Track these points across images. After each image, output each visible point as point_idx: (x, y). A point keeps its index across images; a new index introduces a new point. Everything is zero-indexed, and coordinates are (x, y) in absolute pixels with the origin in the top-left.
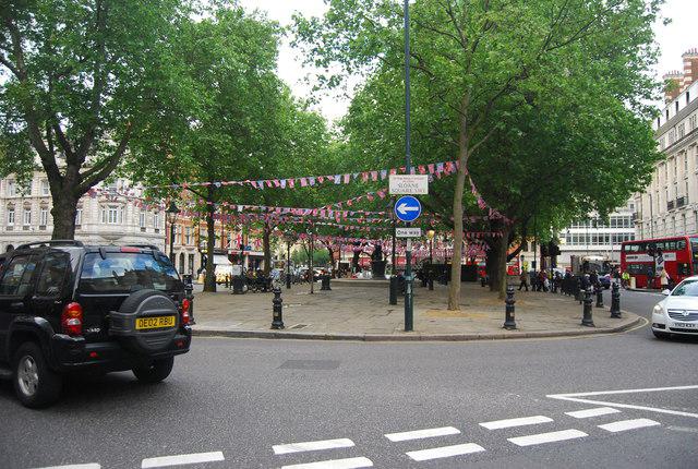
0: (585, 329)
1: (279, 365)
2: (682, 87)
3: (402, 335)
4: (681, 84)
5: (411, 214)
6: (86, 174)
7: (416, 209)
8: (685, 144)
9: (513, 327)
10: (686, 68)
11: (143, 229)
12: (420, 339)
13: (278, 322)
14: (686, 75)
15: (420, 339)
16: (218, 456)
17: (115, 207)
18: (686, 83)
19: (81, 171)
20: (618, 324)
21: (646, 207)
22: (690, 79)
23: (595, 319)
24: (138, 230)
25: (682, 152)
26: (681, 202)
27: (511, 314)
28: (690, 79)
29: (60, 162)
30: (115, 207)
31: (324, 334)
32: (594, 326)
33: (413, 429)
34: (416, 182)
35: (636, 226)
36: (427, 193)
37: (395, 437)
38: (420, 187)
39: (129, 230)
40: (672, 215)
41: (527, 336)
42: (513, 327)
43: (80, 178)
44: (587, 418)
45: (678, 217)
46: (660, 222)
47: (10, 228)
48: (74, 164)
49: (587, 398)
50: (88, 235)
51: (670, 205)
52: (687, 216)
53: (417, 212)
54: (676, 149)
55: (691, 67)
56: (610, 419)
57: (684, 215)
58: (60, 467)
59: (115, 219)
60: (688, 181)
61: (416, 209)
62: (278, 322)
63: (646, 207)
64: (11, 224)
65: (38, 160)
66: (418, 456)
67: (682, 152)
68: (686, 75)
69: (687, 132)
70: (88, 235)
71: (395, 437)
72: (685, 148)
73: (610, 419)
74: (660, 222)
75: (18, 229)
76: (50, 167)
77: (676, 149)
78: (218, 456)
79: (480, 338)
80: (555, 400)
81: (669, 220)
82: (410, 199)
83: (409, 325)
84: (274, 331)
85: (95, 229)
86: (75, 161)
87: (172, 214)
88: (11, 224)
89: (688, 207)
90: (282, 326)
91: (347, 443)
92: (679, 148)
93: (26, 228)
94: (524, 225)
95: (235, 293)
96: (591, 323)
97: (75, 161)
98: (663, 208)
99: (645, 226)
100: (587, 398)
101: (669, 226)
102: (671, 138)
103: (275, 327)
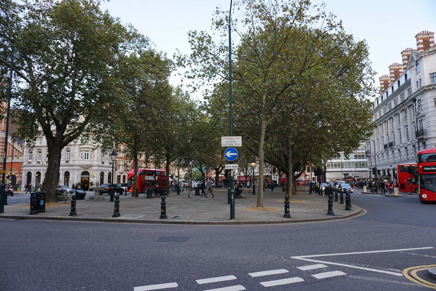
0: (329, 217)
1: (157, 239)
2: (390, 83)
3: (228, 221)
4: (389, 82)
5: (233, 157)
6: (66, 135)
7: (235, 154)
8: (392, 114)
9: (289, 217)
10: (391, 73)
11: (103, 163)
12: (238, 223)
13: (163, 215)
14: (391, 77)
15: (238, 223)
16: (174, 285)
17: (88, 151)
18: (392, 81)
19: (65, 133)
20: (348, 213)
21: (373, 148)
22: (394, 79)
23: (335, 210)
24: (100, 163)
25: (391, 118)
26: (391, 145)
27: (288, 210)
28: (394, 79)
29: (53, 128)
30: (88, 151)
31: (187, 221)
32: (334, 215)
33: (213, 277)
34: (235, 140)
35: (368, 158)
36: (241, 145)
37: (254, 275)
38: (237, 143)
39: (95, 163)
40: (386, 152)
41: (296, 221)
42: (289, 217)
43: (63, 137)
44: (307, 271)
45: (390, 153)
46: (380, 155)
47: (29, 163)
48: (60, 130)
49: (312, 258)
50: (72, 166)
51: (385, 147)
52: (394, 152)
53: (236, 156)
54: (387, 116)
55: (394, 73)
56: (320, 271)
57: (393, 152)
58: (326, 277)
59: (88, 157)
60: (395, 133)
61: (235, 154)
62: (163, 215)
63: (373, 148)
64: (31, 160)
65: (40, 129)
66: (266, 284)
67: (391, 118)
68: (391, 77)
69: (393, 107)
70: (72, 166)
71: (254, 275)
72: (392, 116)
73: (320, 271)
74: (380, 155)
75: (34, 163)
76: (47, 132)
77: (387, 116)
78: (174, 285)
79: (270, 223)
80: (296, 260)
81: (385, 154)
82: (232, 149)
83: (232, 215)
84: (161, 220)
85: (76, 163)
86: (61, 129)
87: (114, 156)
88: (31, 160)
89: (395, 147)
90: (166, 217)
91: (232, 277)
92: (383, 120)
93: (38, 162)
94: (304, 159)
95: (148, 197)
96: (333, 213)
97: (61, 129)
98: (382, 148)
99: (372, 158)
100: (312, 258)
101: (385, 158)
102: (384, 111)
103: (162, 217)
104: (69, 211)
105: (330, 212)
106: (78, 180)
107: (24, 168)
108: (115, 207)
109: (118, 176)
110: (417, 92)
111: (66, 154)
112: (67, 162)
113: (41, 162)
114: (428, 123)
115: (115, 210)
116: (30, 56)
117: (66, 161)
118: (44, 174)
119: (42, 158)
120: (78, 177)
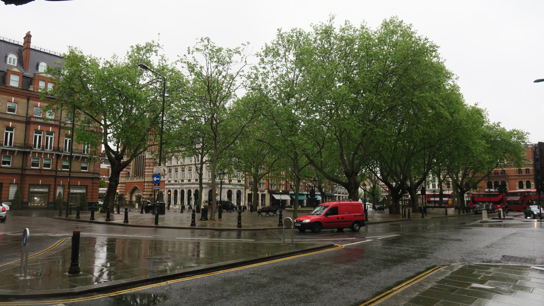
47: (169, 181)
64: (170, 179)
75: (173, 182)
93: (176, 181)
104: (278, 223)
105: (459, 213)
106: (206, 198)
107: (166, 187)
108: (192, 219)
109: (249, 194)
110: (29, 54)
111: (188, 173)
112: (189, 180)
113: (178, 181)
114: (23, 88)
115: (192, 221)
116: (408, 184)
117: (189, 180)
118: (173, 192)
119: (179, 177)
120: (205, 195)
